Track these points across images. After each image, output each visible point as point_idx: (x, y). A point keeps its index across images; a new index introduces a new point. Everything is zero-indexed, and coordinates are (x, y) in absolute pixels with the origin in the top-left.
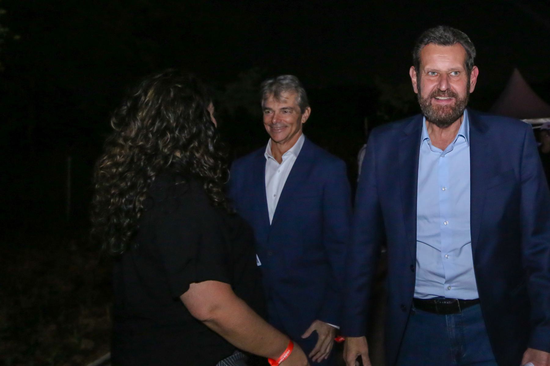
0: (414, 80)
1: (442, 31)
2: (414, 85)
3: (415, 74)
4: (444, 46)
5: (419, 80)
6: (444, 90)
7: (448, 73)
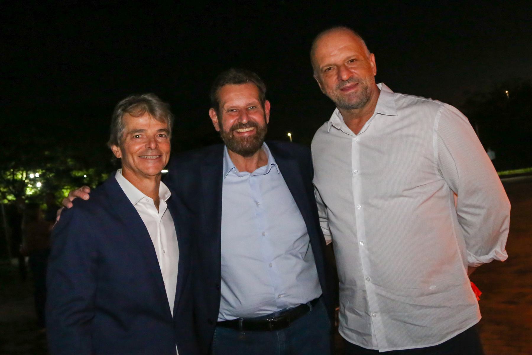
2: (215, 124)
3: (215, 115)
4: (239, 85)
5: (219, 118)
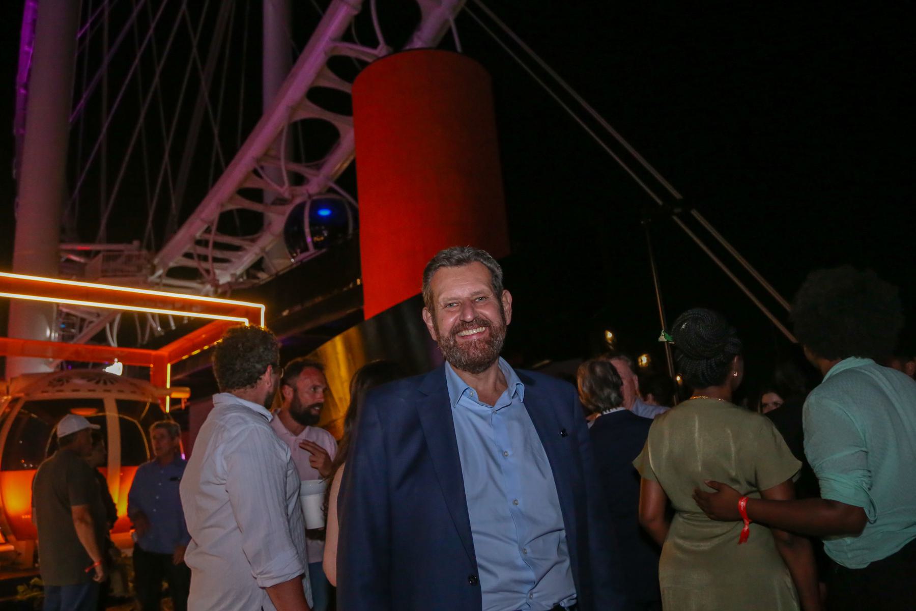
0: (430, 324)
1: (478, 369)
6: (471, 320)
7: (471, 299)
